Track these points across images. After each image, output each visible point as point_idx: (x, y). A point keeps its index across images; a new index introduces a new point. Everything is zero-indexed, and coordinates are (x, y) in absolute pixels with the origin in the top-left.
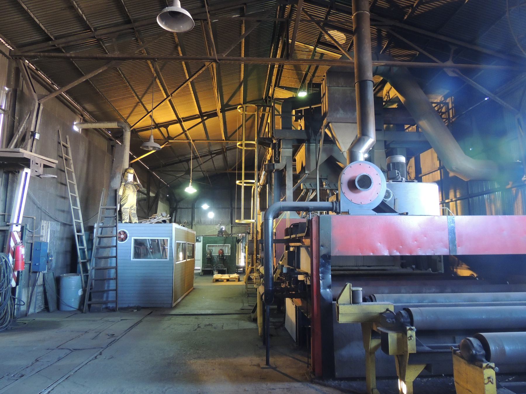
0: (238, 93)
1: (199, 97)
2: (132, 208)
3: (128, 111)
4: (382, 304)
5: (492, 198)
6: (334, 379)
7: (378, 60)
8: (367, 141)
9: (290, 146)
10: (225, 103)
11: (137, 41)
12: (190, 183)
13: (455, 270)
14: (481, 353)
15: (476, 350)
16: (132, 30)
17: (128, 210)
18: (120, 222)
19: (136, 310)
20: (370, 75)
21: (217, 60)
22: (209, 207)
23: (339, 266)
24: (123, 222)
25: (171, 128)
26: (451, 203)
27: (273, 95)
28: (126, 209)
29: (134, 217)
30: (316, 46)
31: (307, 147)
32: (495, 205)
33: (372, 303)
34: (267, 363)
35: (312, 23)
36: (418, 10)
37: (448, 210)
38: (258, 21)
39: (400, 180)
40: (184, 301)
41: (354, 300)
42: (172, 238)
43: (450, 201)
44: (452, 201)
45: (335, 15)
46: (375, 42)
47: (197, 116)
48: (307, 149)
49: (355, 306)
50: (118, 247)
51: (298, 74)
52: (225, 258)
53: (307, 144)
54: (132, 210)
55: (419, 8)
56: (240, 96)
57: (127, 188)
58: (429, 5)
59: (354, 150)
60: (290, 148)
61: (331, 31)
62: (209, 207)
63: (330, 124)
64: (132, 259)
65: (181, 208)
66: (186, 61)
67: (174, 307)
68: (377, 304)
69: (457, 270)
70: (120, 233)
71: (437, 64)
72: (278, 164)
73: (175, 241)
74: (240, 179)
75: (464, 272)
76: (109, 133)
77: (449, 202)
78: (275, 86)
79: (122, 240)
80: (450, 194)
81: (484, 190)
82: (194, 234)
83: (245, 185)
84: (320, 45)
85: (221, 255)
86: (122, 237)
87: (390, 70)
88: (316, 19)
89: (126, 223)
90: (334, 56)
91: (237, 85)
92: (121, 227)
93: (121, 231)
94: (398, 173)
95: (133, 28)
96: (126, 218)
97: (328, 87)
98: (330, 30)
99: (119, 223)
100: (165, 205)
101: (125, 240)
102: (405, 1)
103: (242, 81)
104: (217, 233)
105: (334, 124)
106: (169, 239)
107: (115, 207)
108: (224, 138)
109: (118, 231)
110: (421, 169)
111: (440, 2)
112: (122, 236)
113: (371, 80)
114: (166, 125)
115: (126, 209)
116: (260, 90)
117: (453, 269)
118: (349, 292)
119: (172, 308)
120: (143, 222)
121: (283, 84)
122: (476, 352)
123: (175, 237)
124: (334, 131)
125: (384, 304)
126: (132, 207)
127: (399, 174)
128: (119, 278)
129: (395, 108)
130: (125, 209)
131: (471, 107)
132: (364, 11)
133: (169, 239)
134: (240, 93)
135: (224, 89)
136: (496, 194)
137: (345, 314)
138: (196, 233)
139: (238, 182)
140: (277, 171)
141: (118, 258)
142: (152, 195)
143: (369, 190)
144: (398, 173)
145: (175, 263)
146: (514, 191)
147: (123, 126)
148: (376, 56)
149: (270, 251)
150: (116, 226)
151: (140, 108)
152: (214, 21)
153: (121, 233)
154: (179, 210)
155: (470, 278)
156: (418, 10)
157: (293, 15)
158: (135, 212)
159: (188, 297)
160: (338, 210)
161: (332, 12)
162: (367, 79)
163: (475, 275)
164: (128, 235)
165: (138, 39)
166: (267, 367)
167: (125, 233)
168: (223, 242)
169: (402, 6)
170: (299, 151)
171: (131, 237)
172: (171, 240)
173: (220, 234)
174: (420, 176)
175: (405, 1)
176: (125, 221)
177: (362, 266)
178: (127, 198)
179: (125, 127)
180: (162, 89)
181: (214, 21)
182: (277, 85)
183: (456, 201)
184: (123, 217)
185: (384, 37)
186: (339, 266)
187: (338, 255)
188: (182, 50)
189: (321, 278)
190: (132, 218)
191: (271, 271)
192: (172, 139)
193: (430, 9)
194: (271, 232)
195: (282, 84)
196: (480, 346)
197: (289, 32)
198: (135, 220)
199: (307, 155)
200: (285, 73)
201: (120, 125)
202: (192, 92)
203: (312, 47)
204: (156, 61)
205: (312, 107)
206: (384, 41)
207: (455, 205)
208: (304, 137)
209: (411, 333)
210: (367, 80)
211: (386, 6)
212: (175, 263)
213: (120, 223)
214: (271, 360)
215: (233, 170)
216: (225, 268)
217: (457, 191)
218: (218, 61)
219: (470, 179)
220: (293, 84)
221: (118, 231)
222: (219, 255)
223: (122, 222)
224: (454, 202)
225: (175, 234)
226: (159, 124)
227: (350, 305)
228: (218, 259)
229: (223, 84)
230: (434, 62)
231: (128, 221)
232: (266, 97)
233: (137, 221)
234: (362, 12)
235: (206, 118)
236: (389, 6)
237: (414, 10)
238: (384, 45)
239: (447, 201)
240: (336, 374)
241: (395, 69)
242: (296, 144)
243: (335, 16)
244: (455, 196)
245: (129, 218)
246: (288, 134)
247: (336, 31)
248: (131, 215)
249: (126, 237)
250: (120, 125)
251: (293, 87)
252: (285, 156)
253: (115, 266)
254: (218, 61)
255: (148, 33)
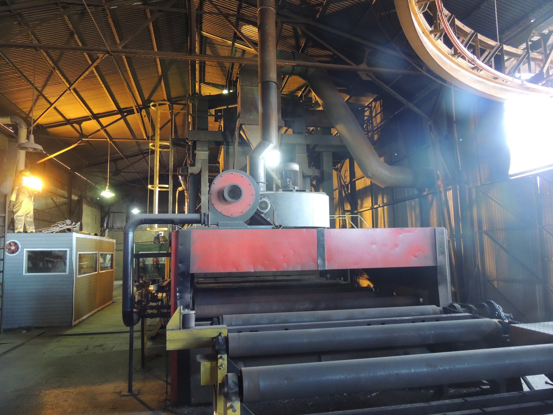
0: (159, 89)
1: (113, 91)
2: (28, 216)
3: (29, 105)
4: (215, 328)
5: (413, 205)
6: (190, 405)
7: (294, 60)
8: (268, 146)
9: (206, 149)
10: (146, 99)
11: (20, 25)
12: (107, 187)
13: (358, 280)
14: (234, 391)
15: (229, 388)
16: (9, 13)
17: (23, 218)
18: (13, 231)
19: (26, 331)
20: (273, 76)
21: (110, 52)
22: (132, 211)
23: (256, 276)
24: (16, 231)
25: (85, 124)
26: (379, 209)
27: (200, 92)
28: (20, 216)
29: (29, 226)
30: (234, 41)
31: (225, 149)
32: (415, 211)
33: (219, 325)
34: (130, 390)
35: (220, 16)
36: (328, 8)
37: (360, 218)
38: (159, 11)
39: (291, 189)
40: (91, 318)
41: (185, 323)
42: (72, 249)
43: (378, 206)
44: (380, 207)
45: (248, 9)
46: (293, 40)
47: (115, 112)
48: (225, 152)
49: (185, 331)
50: (6, 261)
51: (222, 70)
52: (160, 266)
53: (225, 147)
54: (29, 217)
55: (329, 6)
56: (162, 91)
57: (21, 193)
58: (339, 5)
59: (254, 156)
60: (206, 151)
61: (246, 26)
62: (132, 211)
63: (243, 126)
64: (24, 274)
65: (114, 212)
66: (89, 52)
67: (74, 325)
68: (209, 329)
69: (359, 280)
70: (10, 244)
71: (351, 66)
72: (193, 168)
73: (77, 252)
74: (152, 183)
75: (365, 283)
76: (10, 129)
77: (377, 208)
78: (200, 82)
79: (13, 252)
80: (379, 199)
81: (406, 196)
82: (114, 242)
83: (160, 189)
84: (239, 40)
85: (155, 263)
86: (13, 249)
87: (307, 70)
88: (225, 11)
89: (19, 232)
90: (251, 52)
91: (156, 80)
92: (10, 238)
93: (12, 242)
94: (289, 182)
95: (10, 11)
96: (20, 227)
97: (241, 86)
98: (246, 25)
99: (8, 233)
100: (94, 209)
101: (16, 252)
102: (228, 1)
103: (161, 75)
104: (153, 240)
105: (247, 126)
106: (68, 250)
107: (4, 215)
108: (145, 137)
109: (7, 242)
110: (355, 173)
111: (348, 2)
112: (13, 248)
113: (274, 81)
114: (79, 121)
115: (20, 216)
116: (184, 85)
117: (357, 279)
118: (179, 316)
119: (71, 326)
120: (43, 231)
121: (208, 79)
122: (228, 390)
123: (76, 248)
124: (247, 133)
125: (217, 328)
126: (28, 214)
127: (290, 183)
128: (5, 295)
129: (321, 110)
130: (18, 217)
131: (396, 111)
132: (268, 6)
133: (68, 250)
134: (162, 87)
135: (142, 83)
136: (406, 203)
137: (173, 341)
138: (116, 241)
139: (150, 187)
140: (192, 174)
141: (5, 272)
142: (75, 198)
143: (239, 201)
144: (289, 182)
145: (76, 277)
146: (430, 198)
147: (18, 122)
148: (281, 55)
149: (130, 268)
150: (4, 237)
151: (42, 101)
152: (112, 8)
153: (12, 244)
154: (111, 215)
155: (368, 288)
156: (328, 8)
157: (204, 7)
158: (32, 220)
159: (98, 313)
160: (206, 223)
161: (244, 5)
162: (269, 80)
163: (372, 286)
164: (20, 246)
165: (21, 23)
166: (129, 394)
167: (16, 244)
168: (158, 249)
169: (312, 4)
170: (221, 154)
171: (23, 249)
172: (71, 251)
173: (157, 240)
174: (354, 180)
175: (228, 1)
176: (18, 230)
177: (280, 276)
178: (21, 205)
179: (20, 123)
180: (64, 80)
181: (112, 8)
182: (202, 80)
183: (383, 206)
184: (16, 226)
185: (301, 35)
186: (256, 276)
187: (198, 272)
188: (79, 38)
189: (178, 298)
190: (27, 227)
191: (129, 290)
192: (86, 137)
193: (341, 8)
194: (131, 247)
195: (207, 79)
196: (235, 383)
197: (235, 21)
198: (31, 229)
199: (225, 158)
200: (208, 69)
201: (13, 120)
202: (103, 86)
203: (231, 42)
204: (38, 50)
205: (229, 107)
206: (302, 40)
207: (382, 211)
208: (220, 138)
209: (223, 361)
210: (269, 81)
211: (297, 3)
212: (76, 277)
213: (13, 233)
214: (136, 386)
215: (166, 172)
216: (160, 277)
217: (385, 196)
218: (112, 53)
219: (386, 186)
220: (220, 80)
221: (7, 242)
222: (153, 263)
223: (14, 232)
224: (382, 208)
225: (76, 245)
226: (70, 120)
227: (179, 331)
228: (153, 268)
229: (139, 78)
230: (349, 64)
231: (22, 230)
232: (193, 94)
233: (34, 231)
234: (266, 8)
235: (125, 114)
236: (300, 3)
237: (325, 8)
238: (303, 44)
239: (375, 206)
240: (193, 399)
241: (311, 71)
242: (213, 146)
243: (248, 10)
244: (383, 202)
245: (23, 227)
246: (202, 136)
247: (252, 26)
248: (27, 223)
249: (18, 249)
250: (13, 120)
251: (219, 83)
252: (200, 159)
253: (2, 282)
254: (112, 53)
255: (33, 17)
